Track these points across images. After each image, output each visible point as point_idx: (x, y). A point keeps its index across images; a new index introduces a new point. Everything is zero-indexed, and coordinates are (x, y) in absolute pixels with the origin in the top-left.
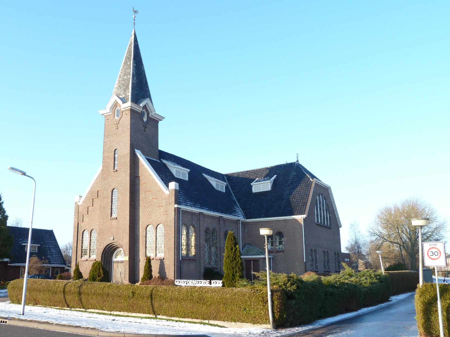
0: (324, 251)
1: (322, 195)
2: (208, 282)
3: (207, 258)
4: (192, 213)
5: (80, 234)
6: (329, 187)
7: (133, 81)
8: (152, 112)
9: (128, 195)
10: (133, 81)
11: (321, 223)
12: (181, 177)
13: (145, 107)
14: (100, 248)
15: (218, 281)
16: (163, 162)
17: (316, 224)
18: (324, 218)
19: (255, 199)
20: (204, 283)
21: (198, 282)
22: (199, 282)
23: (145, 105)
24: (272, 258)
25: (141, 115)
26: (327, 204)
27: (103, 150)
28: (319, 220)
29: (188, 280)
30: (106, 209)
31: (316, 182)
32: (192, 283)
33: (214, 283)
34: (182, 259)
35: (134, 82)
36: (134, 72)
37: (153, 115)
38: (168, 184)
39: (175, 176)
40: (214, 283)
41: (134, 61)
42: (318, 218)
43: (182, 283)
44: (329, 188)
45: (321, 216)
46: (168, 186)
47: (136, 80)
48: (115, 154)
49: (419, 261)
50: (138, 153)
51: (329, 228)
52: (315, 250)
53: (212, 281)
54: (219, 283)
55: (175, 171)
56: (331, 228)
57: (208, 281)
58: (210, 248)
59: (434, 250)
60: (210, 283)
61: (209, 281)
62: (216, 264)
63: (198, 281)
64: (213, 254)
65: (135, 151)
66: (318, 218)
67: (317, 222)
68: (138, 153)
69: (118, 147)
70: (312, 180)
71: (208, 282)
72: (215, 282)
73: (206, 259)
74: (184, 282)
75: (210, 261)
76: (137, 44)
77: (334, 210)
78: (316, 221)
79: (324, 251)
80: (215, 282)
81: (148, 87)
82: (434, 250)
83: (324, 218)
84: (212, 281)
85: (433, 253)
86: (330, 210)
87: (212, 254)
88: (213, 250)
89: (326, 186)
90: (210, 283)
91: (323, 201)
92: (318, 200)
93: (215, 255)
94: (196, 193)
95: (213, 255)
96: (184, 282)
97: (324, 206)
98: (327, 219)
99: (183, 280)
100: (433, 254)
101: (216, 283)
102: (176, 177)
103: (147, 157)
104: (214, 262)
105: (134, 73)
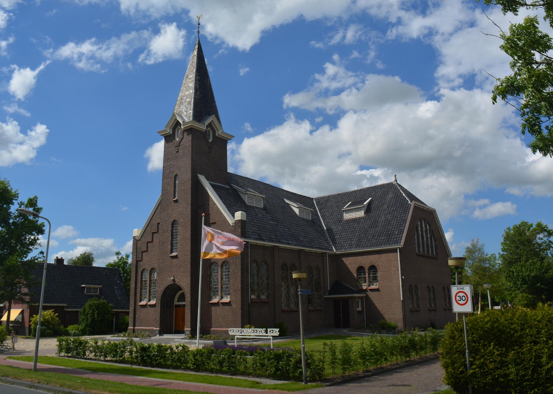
0: (428, 287)
1: (425, 220)
2: (264, 330)
3: (284, 299)
4: (264, 247)
5: (139, 274)
6: (434, 210)
7: (196, 97)
8: (218, 130)
9: (189, 228)
10: (196, 97)
11: (419, 251)
12: (255, 204)
13: (210, 125)
14: (160, 290)
15: (275, 329)
16: (234, 187)
17: (417, 255)
18: (428, 247)
19: (346, 227)
20: (260, 332)
21: (253, 331)
22: (254, 331)
23: (210, 123)
24: (365, 296)
25: (204, 135)
26: (432, 230)
27: (163, 175)
28: (421, 250)
29: (243, 329)
30: (165, 245)
31: (416, 205)
32: (247, 332)
33: (270, 332)
34: (252, 302)
35: (198, 98)
36: (197, 86)
37: (221, 133)
38: (234, 214)
39: (247, 203)
40: (270, 332)
41: (197, 74)
42: (419, 247)
43: (236, 331)
44: (434, 211)
45: (423, 246)
46: (233, 216)
47: (200, 95)
48: (175, 181)
49: (128, 375)
50: (203, 179)
51: (435, 258)
52: (416, 286)
53: (269, 330)
54: (276, 332)
55: (247, 199)
56: (437, 259)
57: (263, 329)
58: (288, 287)
59: (461, 294)
60: (266, 332)
61: (265, 329)
62: (296, 305)
63: (253, 330)
64: (292, 294)
65: (198, 176)
66: (419, 247)
67: (418, 251)
68: (203, 179)
69: (179, 173)
70: (411, 203)
71: (264, 330)
72: (272, 330)
73: (283, 300)
74: (238, 331)
75: (288, 303)
76: (201, 54)
77: (441, 237)
78: (417, 251)
79: (428, 286)
80: (272, 330)
81: (214, 102)
82: (461, 294)
83: (428, 247)
84: (268, 329)
85: (460, 298)
86: (435, 236)
87: (291, 294)
88: (292, 289)
89: (429, 209)
90: (266, 332)
91: (426, 226)
92: (420, 225)
93: (294, 295)
94: (272, 222)
95: (292, 295)
96: (238, 331)
97: (427, 233)
98: (432, 248)
99: (237, 329)
100: (461, 299)
101: (272, 331)
102: (248, 204)
103: (211, 182)
104: (294, 303)
105: (198, 88)
